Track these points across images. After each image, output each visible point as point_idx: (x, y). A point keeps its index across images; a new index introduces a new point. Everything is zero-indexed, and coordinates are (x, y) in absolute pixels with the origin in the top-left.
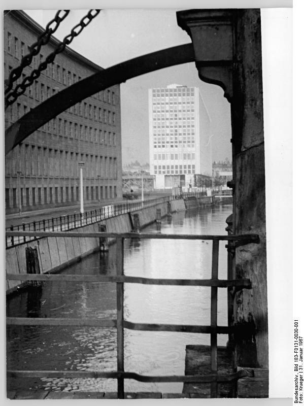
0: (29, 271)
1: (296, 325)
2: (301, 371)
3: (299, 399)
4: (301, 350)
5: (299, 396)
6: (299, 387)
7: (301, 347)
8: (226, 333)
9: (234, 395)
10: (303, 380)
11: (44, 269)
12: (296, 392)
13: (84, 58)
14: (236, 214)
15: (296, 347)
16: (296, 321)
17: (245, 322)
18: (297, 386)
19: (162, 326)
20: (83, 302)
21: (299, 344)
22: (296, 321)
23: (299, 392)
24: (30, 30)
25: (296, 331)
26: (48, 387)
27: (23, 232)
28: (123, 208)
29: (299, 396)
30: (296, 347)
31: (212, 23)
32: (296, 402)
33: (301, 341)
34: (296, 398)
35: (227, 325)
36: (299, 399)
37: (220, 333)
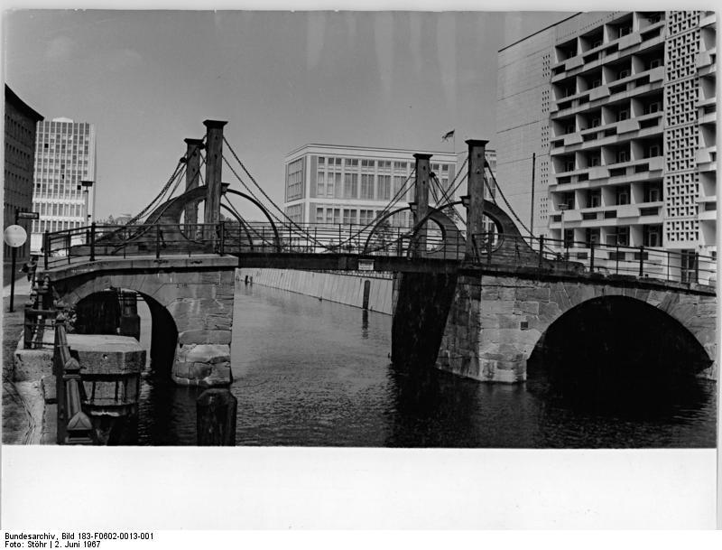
0: (395, 163)
1: (145, 536)
2: (54, 544)
3: (13, 541)
4: (19, 545)
5: (17, 541)
7: (82, 544)
9: (228, 440)
12: (25, 537)
15: (130, 536)
16: (150, 536)
17: (700, 370)
18: (35, 537)
19: (368, 299)
20: (191, 297)
21: (87, 541)
22: (150, 536)
23: (25, 542)
25: (106, 536)
26: (195, 306)
28: (280, 236)
29: (17, 541)
30: (130, 536)
31: (57, 264)
32: (7, 536)
33: (92, 544)
36: (13, 541)
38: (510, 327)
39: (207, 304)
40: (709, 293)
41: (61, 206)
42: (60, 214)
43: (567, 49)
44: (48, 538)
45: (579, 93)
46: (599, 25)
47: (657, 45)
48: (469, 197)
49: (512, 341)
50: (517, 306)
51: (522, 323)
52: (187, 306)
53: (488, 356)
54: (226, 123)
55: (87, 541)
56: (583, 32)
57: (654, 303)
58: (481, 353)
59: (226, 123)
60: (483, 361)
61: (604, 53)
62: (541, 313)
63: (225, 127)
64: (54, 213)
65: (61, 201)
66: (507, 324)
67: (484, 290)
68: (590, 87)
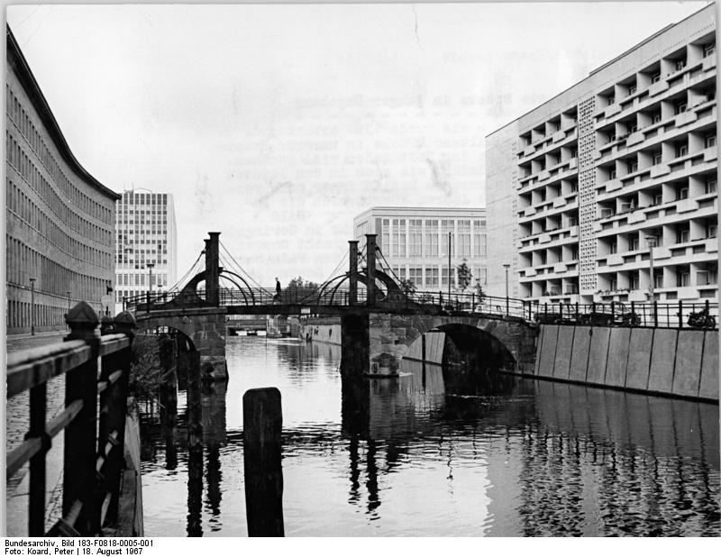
2: (81, 551)
3: (13, 548)
5: (17, 548)
6: (34, 548)
8: (244, 427)
10: (108, 555)
11: (270, 347)
12: (25, 544)
13: (29, 69)
14: (214, 274)
15: (109, 543)
16: (150, 543)
18: (35, 544)
21: (129, 548)
22: (150, 543)
23: (25, 549)
24: (675, 83)
27: (709, 299)
29: (17, 548)
30: (109, 543)
32: (7, 543)
34: (14, 543)
35: (228, 429)
36: (13, 548)
37: (225, 425)
38: (388, 343)
39: (211, 334)
40: (717, 330)
41: (126, 276)
42: (126, 283)
43: (527, 137)
44: (48, 544)
45: (665, 118)
46: (542, 123)
47: (681, 92)
48: (367, 269)
49: (390, 351)
50: (392, 331)
51: (84, 308)
52: (200, 334)
53: (374, 360)
54: (219, 233)
55: (129, 548)
56: (666, 54)
57: (482, 328)
58: (371, 358)
59: (219, 233)
60: (371, 363)
61: (638, 99)
62: (407, 334)
63: (220, 236)
64: (137, 283)
65: (126, 271)
66: (386, 342)
67: (371, 323)
68: (677, 113)
